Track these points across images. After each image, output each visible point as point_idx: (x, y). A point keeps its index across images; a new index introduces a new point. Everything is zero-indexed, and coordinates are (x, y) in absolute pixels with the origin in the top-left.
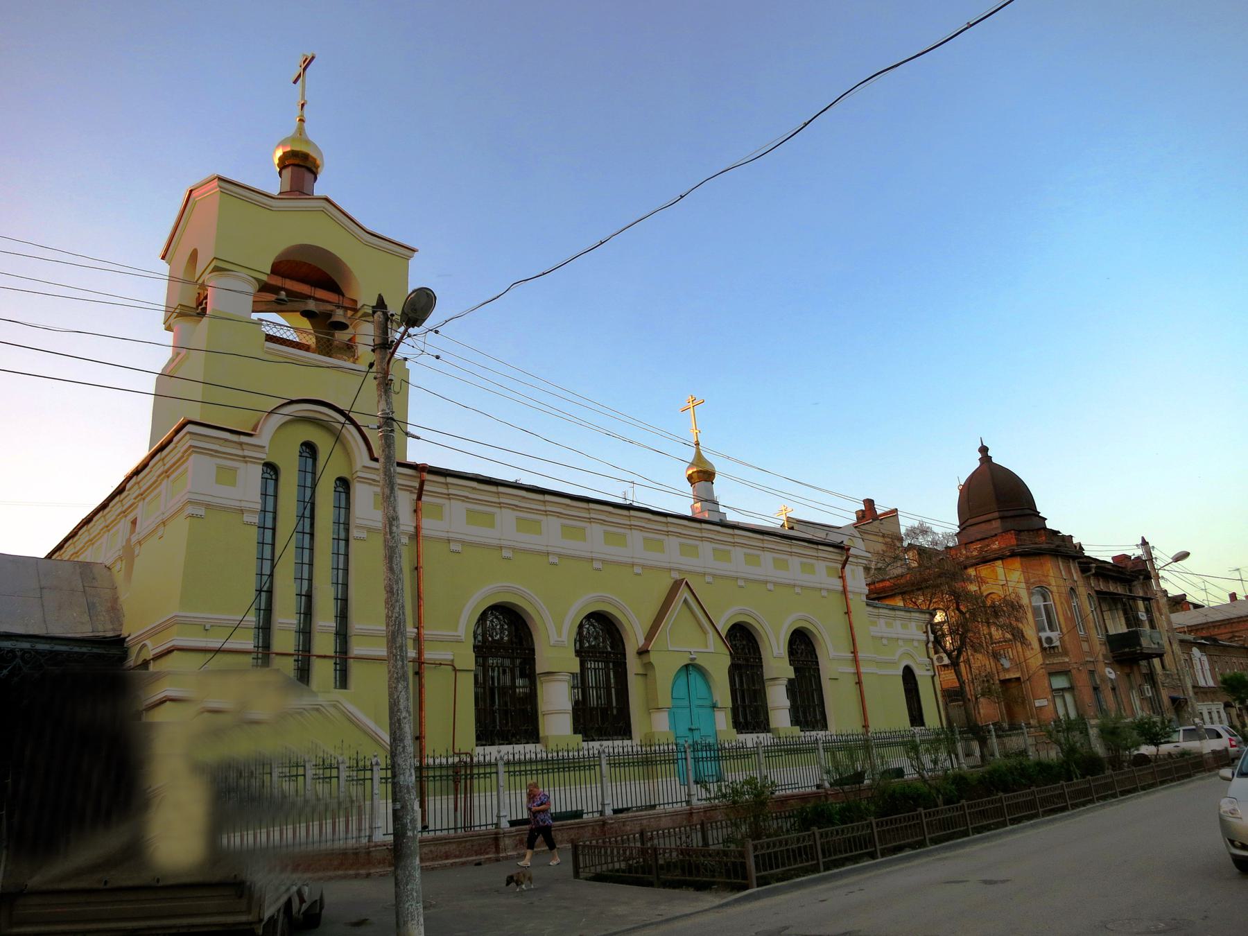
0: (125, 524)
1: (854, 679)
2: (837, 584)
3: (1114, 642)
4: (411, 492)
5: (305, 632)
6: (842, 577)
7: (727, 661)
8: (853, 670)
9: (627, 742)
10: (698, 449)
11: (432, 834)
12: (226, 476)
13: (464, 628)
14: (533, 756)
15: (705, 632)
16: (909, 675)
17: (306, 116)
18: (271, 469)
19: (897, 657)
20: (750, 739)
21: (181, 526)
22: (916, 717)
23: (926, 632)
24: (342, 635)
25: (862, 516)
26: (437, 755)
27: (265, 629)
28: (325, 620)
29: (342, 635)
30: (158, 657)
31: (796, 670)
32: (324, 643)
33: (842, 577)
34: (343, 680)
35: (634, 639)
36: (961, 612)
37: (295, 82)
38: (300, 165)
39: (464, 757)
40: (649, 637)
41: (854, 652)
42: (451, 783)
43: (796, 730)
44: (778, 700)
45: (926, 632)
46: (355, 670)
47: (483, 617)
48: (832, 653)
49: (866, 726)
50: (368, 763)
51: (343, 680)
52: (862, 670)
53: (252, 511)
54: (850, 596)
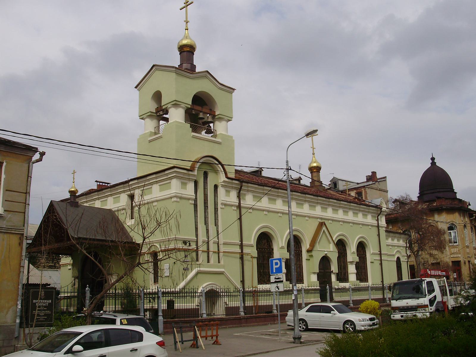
1: (379, 262)
2: (376, 222)
4: (237, 190)
6: (378, 220)
11: (216, 316)
12: (184, 185)
14: (265, 290)
18: (196, 183)
19: (394, 253)
20: (342, 285)
25: (369, 179)
33: (378, 220)
36: (419, 234)
41: (380, 251)
42: (252, 297)
44: (352, 269)
45: (406, 243)
49: (382, 281)
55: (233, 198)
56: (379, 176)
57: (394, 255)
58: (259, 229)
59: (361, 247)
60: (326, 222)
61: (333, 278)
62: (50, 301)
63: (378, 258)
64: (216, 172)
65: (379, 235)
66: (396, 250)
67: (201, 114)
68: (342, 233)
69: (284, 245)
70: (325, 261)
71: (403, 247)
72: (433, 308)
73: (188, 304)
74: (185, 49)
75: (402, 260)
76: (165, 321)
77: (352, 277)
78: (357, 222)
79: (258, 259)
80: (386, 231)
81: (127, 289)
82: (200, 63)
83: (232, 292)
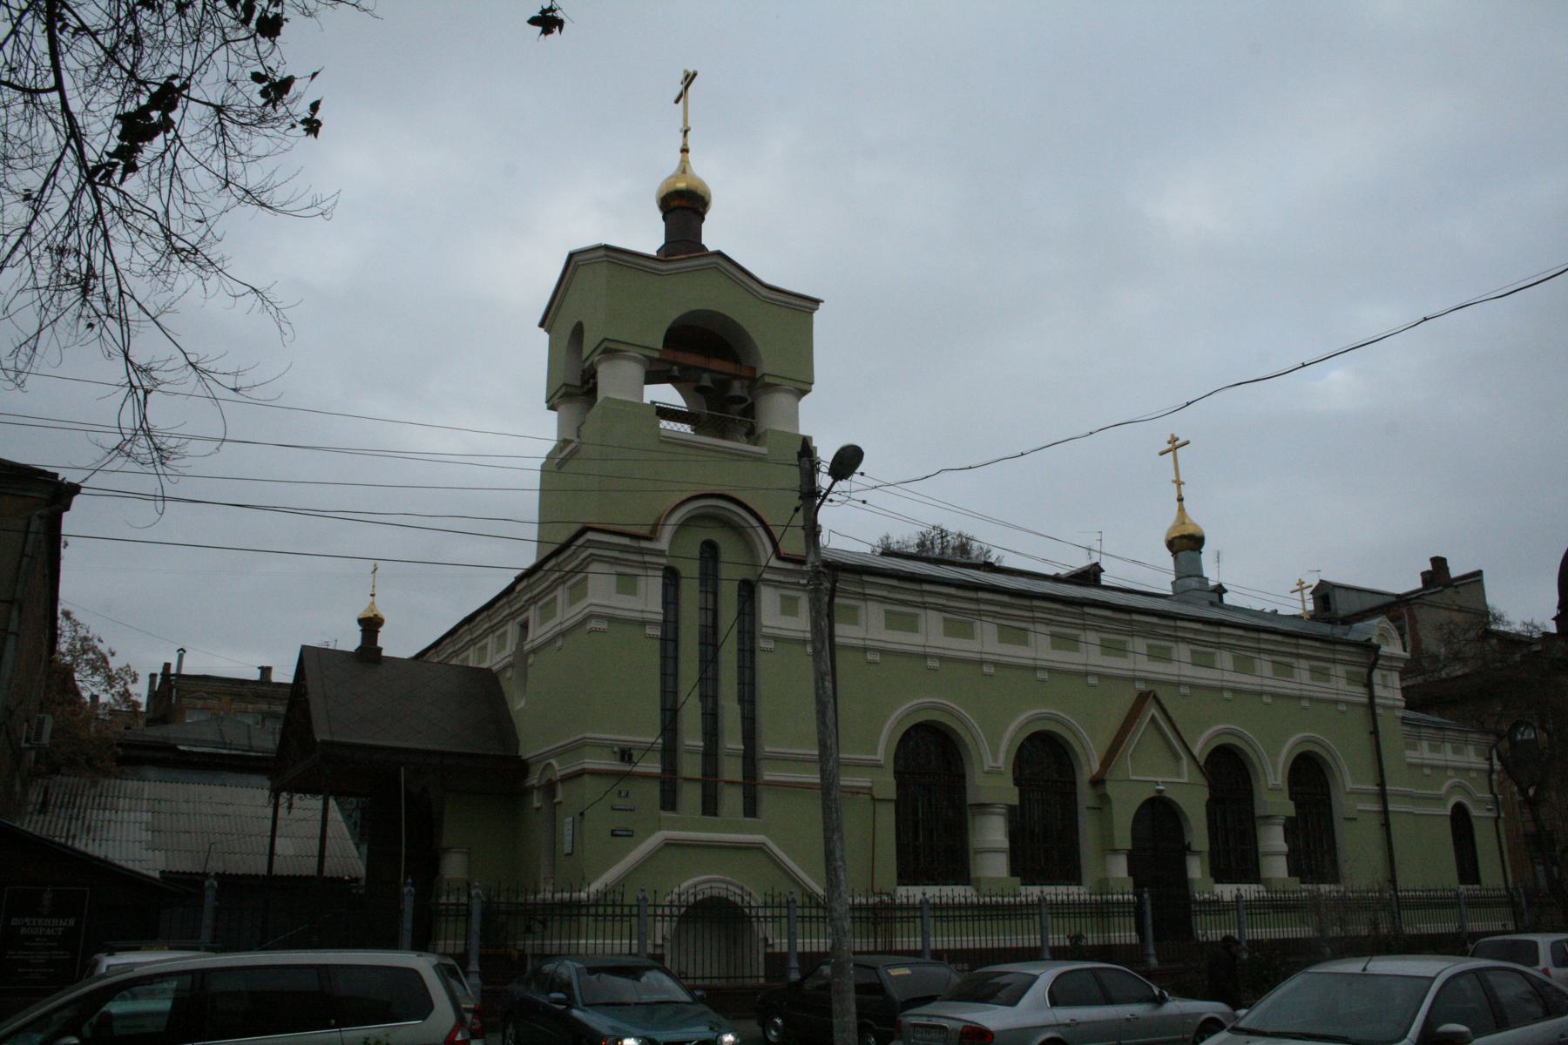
0: (512, 629)
5: (711, 754)
7: (1204, 794)
8: (1377, 807)
9: (1073, 889)
10: (1181, 510)
12: (627, 584)
13: (883, 750)
15: (1177, 757)
16: (1460, 817)
17: (690, 146)
18: (672, 577)
19: (1443, 791)
20: (1227, 891)
22: (1468, 870)
23: (1490, 759)
24: (750, 758)
27: (670, 752)
28: (732, 742)
29: (750, 758)
30: (567, 779)
31: (1298, 806)
32: (732, 769)
33: (1369, 685)
34: (751, 809)
35: (1090, 766)
37: (677, 101)
38: (684, 207)
39: (885, 898)
40: (1107, 762)
41: (1382, 785)
43: (1295, 883)
44: (1274, 840)
45: (1490, 759)
46: (766, 800)
47: (906, 736)
48: (1350, 785)
50: (784, 900)
51: (751, 809)
52: (1391, 808)
53: (652, 623)
54: (1379, 711)
56: (1455, 571)
57: (1439, 800)
58: (1029, 722)
60: (1161, 693)
61: (1196, 869)
62: (72, 922)
66: (1449, 783)
67: (737, 384)
68: (1022, 718)
69: (1279, 781)
71: (1478, 770)
74: (674, 204)
75: (1474, 812)
77: (1276, 867)
78: (626, 613)
79: (903, 806)
82: (714, 234)
83: (631, 906)
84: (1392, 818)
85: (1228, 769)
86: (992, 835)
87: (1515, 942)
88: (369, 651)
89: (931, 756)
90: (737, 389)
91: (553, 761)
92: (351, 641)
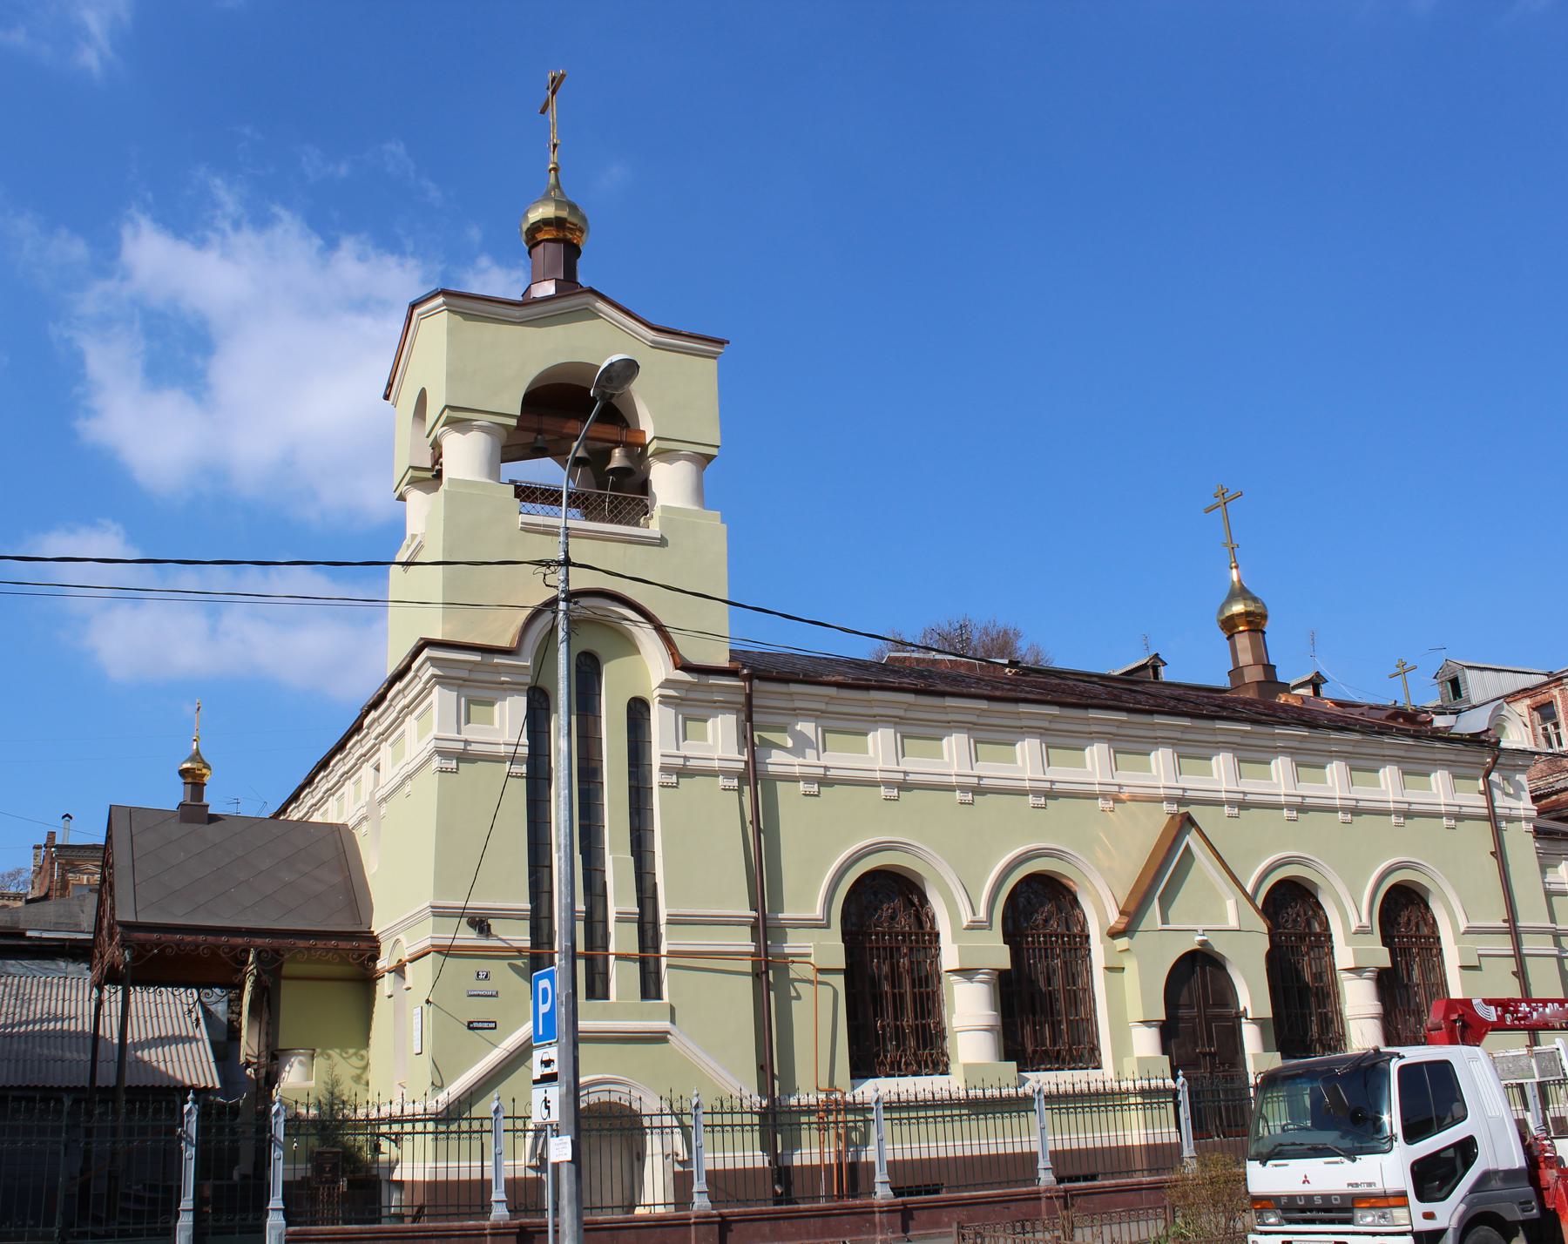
1: (1511, 965)
3: (258, 1113)
21: (429, 781)
26: (1003, 1084)
28: (620, 899)
32: (622, 938)
34: (650, 987)
51: (650, 987)
55: (719, 738)
59: (1403, 909)
60: (1194, 811)
63: (1505, 945)
64: (629, 646)
65: (1499, 854)
67: (617, 452)
70: (1197, 975)
72: (1448, 1213)
73: (1113, 1133)
76: (294, 1234)
80: (1539, 833)
81: (332, 1105)
84: (1530, 963)
85: (1291, 907)
86: (968, 1013)
87: (175, 1194)
88: (194, 812)
89: (885, 909)
90: (618, 458)
91: (400, 936)
92: (173, 795)
